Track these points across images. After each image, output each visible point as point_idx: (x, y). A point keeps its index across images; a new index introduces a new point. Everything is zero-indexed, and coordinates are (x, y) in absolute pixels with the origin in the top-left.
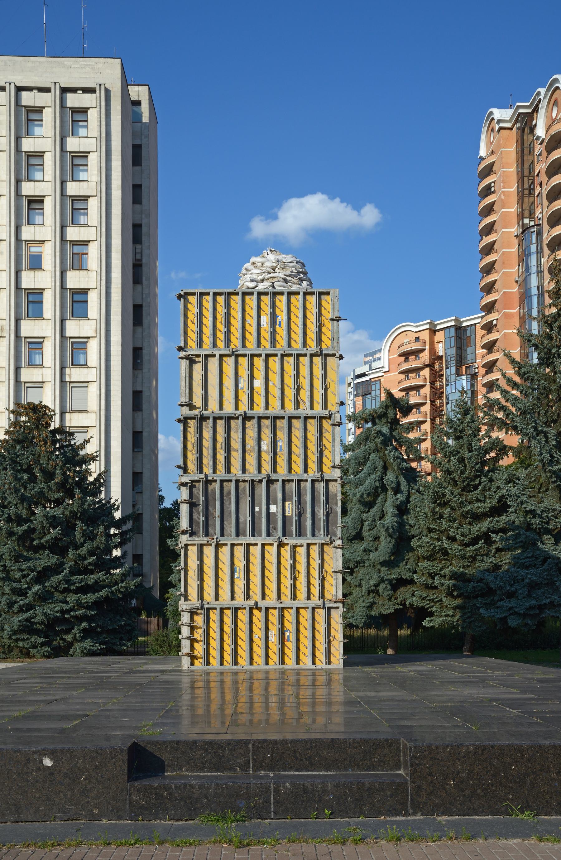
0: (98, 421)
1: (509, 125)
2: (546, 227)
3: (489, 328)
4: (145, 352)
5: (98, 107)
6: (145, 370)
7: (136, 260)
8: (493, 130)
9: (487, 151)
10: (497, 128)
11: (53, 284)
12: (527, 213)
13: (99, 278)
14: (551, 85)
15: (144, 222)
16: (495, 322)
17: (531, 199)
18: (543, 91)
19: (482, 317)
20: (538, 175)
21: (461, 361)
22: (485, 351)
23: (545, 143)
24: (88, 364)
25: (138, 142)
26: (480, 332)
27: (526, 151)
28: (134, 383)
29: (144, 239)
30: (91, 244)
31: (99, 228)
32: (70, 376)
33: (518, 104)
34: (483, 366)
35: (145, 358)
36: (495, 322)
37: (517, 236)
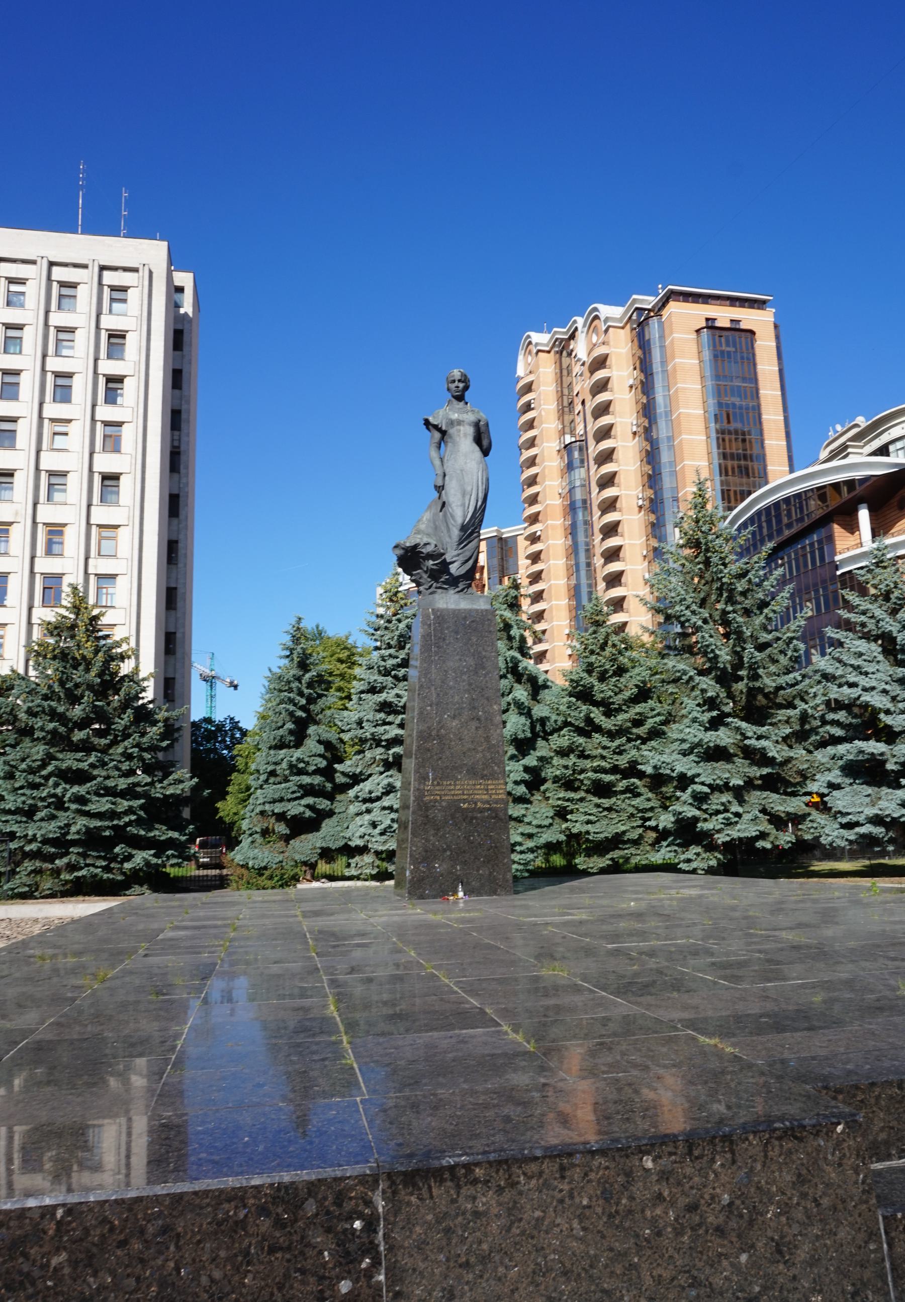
0: (128, 618)
1: (547, 349)
2: (591, 442)
3: (534, 539)
4: (180, 545)
5: (140, 286)
6: (180, 565)
7: (173, 447)
8: (530, 353)
9: (525, 370)
10: (535, 351)
11: (80, 466)
12: (567, 430)
13: (133, 462)
14: (590, 313)
15: (184, 408)
16: (538, 534)
17: (571, 417)
18: (580, 321)
19: (525, 529)
20: (577, 395)
21: (503, 572)
22: (529, 562)
23: (587, 365)
24: (118, 556)
25: (180, 327)
26: (522, 543)
27: (565, 372)
28: (168, 578)
29: (183, 425)
30: (125, 426)
31: (135, 409)
32: (96, 567)
33: (555, 329)
34: (528, 577)
35: (181, 552)
36: (538, 534)
37: (559, 451)
